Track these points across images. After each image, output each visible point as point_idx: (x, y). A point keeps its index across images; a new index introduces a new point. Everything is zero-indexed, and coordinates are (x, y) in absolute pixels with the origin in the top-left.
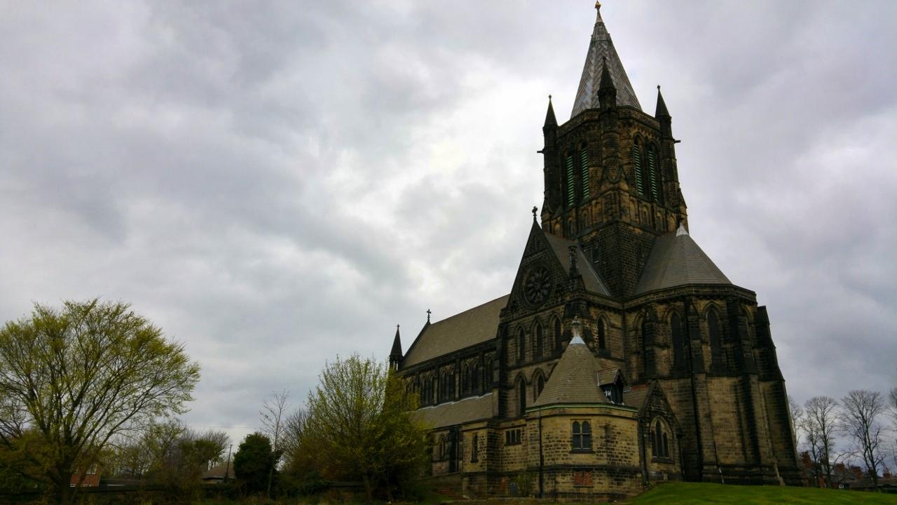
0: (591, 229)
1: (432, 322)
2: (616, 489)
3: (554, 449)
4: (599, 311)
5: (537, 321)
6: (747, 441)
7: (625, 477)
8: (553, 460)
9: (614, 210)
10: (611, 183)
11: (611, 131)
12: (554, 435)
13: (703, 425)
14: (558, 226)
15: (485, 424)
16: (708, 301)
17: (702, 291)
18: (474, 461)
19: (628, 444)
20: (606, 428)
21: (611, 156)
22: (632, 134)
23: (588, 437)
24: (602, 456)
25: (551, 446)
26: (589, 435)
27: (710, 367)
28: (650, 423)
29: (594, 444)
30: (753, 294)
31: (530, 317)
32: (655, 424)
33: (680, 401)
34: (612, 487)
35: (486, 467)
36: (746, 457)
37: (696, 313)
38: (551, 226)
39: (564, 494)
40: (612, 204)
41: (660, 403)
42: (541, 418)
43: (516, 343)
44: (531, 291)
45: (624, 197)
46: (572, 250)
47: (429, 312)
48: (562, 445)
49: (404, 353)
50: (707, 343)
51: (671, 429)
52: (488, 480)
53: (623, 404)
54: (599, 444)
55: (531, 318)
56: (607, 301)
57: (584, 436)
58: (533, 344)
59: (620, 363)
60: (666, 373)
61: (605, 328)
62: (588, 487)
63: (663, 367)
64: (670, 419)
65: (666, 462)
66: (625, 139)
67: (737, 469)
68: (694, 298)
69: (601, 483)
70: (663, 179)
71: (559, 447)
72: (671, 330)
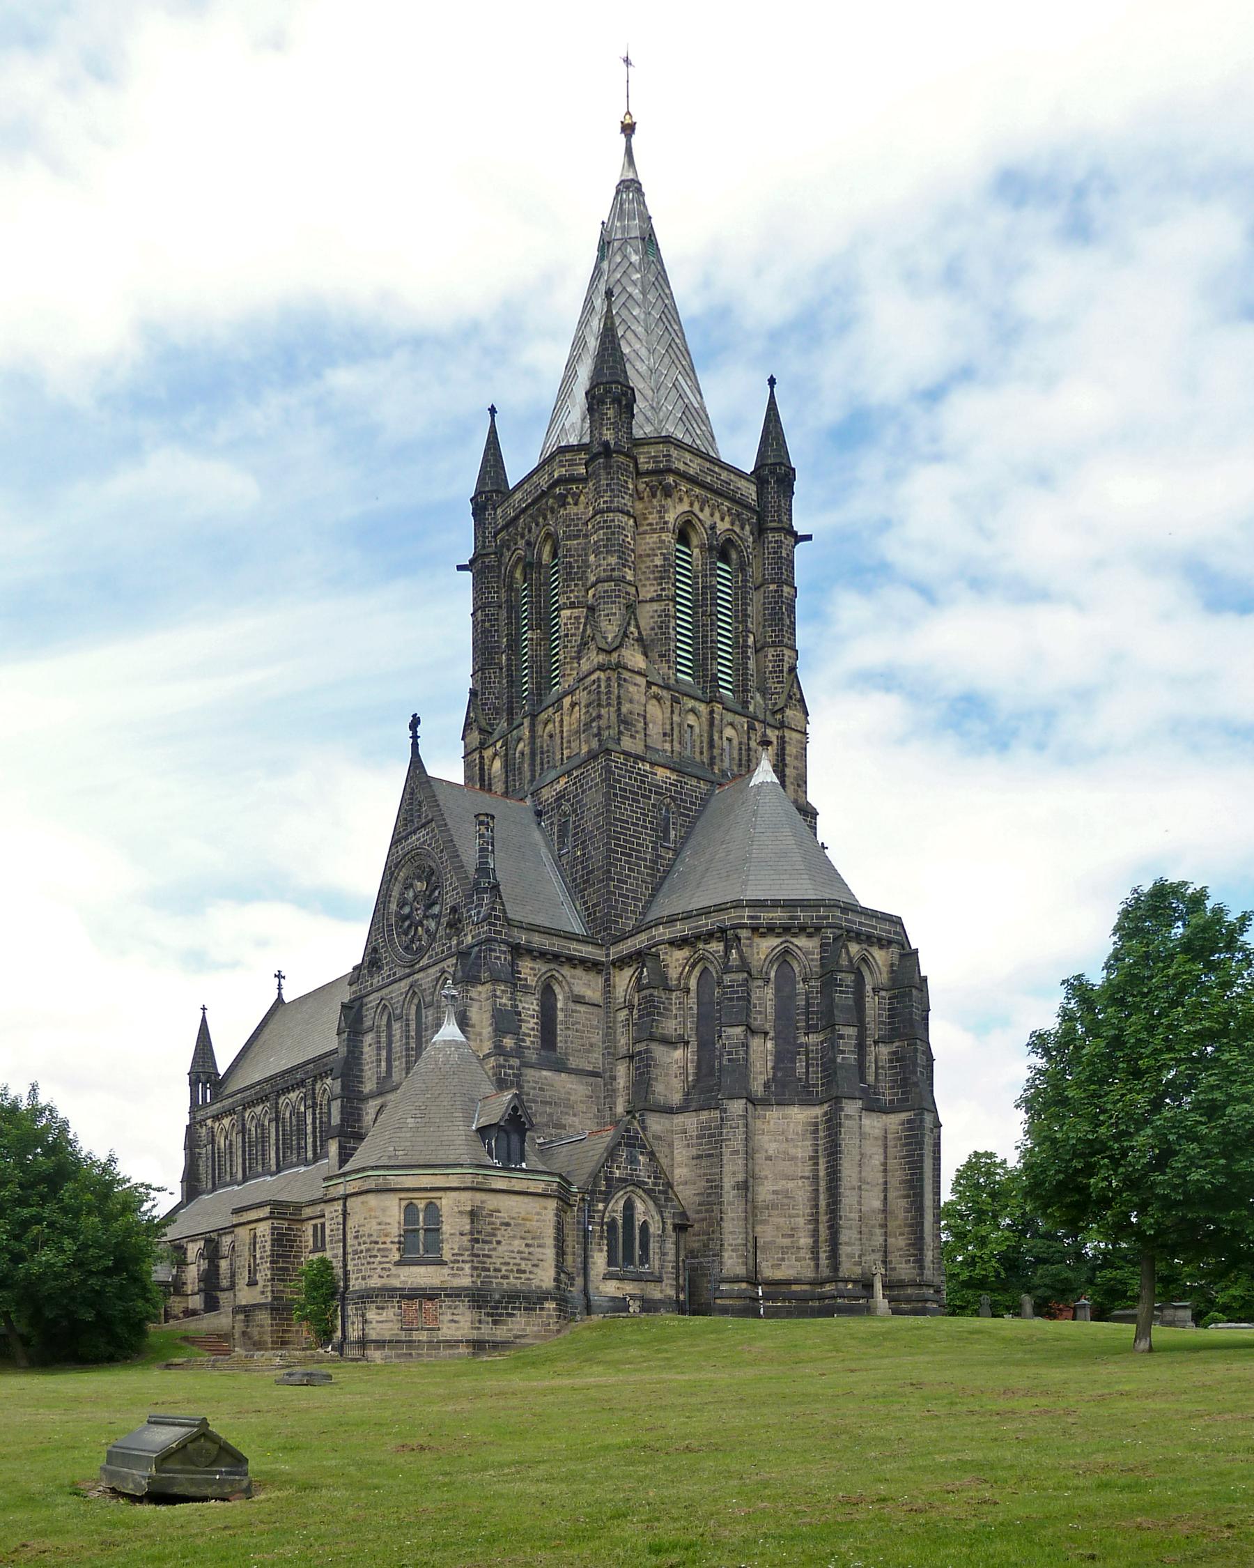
0: (559, 770)
1: (287, 998)
2: (488, 1331)
3: (365, 1258)
4: (542, 967)
5: (415, 993)
6: (824, 1232)
7: (513, 1308)
8: (364, 1278)
9: (603, 723)
10: (600, 650)
11: (609, 510)
12: (366, 1230)
13: (729, 1204)
14: (497, 764)
15: (265, 1212)
16: (779, 940)
17: (766, 916)
18: (252, 1283)
19: (527, 1245)
20: (474, 1214)
21: (609, 579)
22: (671, 517)
23: (434, 1230)
24: (462, 1269)
25: (361, 1252)
26: (438, 1230)
27: (767, 1085)
28: (606, 1202)
29: (446, 1246)
30: (897, 922)
31: (403, 983)
32: (622, 1203)
33: (699, 1157)
34: (479, 1329)
35: (269, 1294)
36: (817, 1266)
37: (744, 967)
38: (482, 764)
39: (380, 1344)
40: (599, 705)
41: (637, 1162)
42: (345, 1198)
43: (379, 1042)
44: (407, 923)
45: (632, 689)
46: (481, 823)
47: (279, 976)
48: (379, 1250)
49: (222, 1068)
50: (766, 1034)
51: (661, 1213)
52: (273, 1319)
53: (524, 1165)
54: (456, 1247)
55: (404, 985)
56: (563, 943)
57: (426, 1230)
58: (408, 1043)
59: (591, 1079)
60: (676, 1098)
61: (559, 1005)
62: (428, 1330)
63: (670, 1088)
64: (662, 1192)
65: (638, 1278)
66: (654, 531)
67: (794, 1288)
68: (744, 933)
69: (455, 1322)
70: (751, 640)
71: (375, 1253)
72: (695, 1007)
